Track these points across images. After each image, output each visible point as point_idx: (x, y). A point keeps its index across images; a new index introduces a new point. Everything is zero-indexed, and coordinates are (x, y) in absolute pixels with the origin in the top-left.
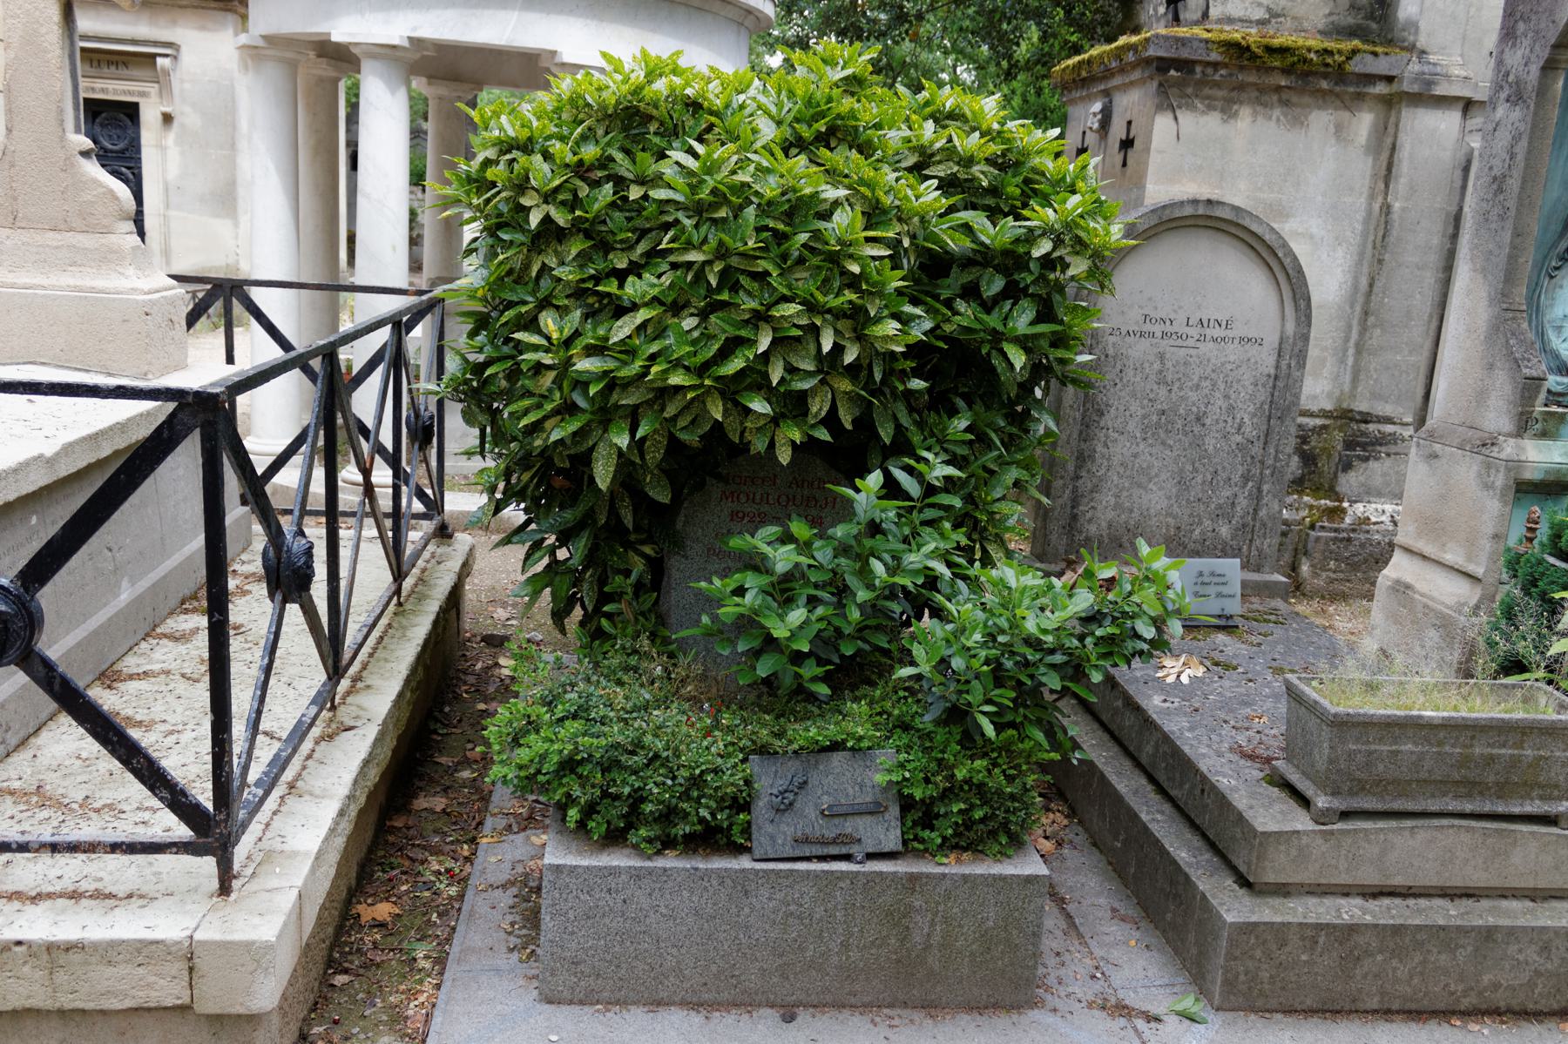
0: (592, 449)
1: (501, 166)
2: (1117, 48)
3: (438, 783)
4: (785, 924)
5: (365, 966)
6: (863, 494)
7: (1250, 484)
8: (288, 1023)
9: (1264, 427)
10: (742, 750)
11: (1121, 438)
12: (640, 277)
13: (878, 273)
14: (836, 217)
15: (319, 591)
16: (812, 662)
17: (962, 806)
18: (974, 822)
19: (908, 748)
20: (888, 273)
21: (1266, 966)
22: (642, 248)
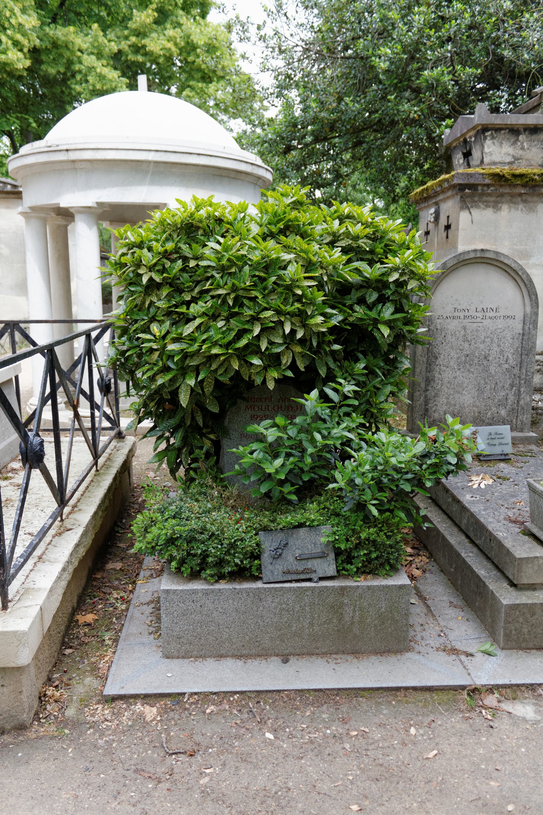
0: (178, 388)
1: (129, 256)
2: (439, 181)
3: (118, 556)
4: (281, 614)
5: (80, 645)
6: (309, 401)
7: (514, 388)
8: (41, 673)
9: (519, 360)
10: (255, 529)
11: (447, 369)
12: (197, 303)
13: (312, 294)
14: (289, 268)
15: (50, 461)
16: (288, 485)
17: (366, 552)
18: (372, 560)
19: (338, 524)
20: (316, 293)
21: (526, 626)
22: (197, 290)
